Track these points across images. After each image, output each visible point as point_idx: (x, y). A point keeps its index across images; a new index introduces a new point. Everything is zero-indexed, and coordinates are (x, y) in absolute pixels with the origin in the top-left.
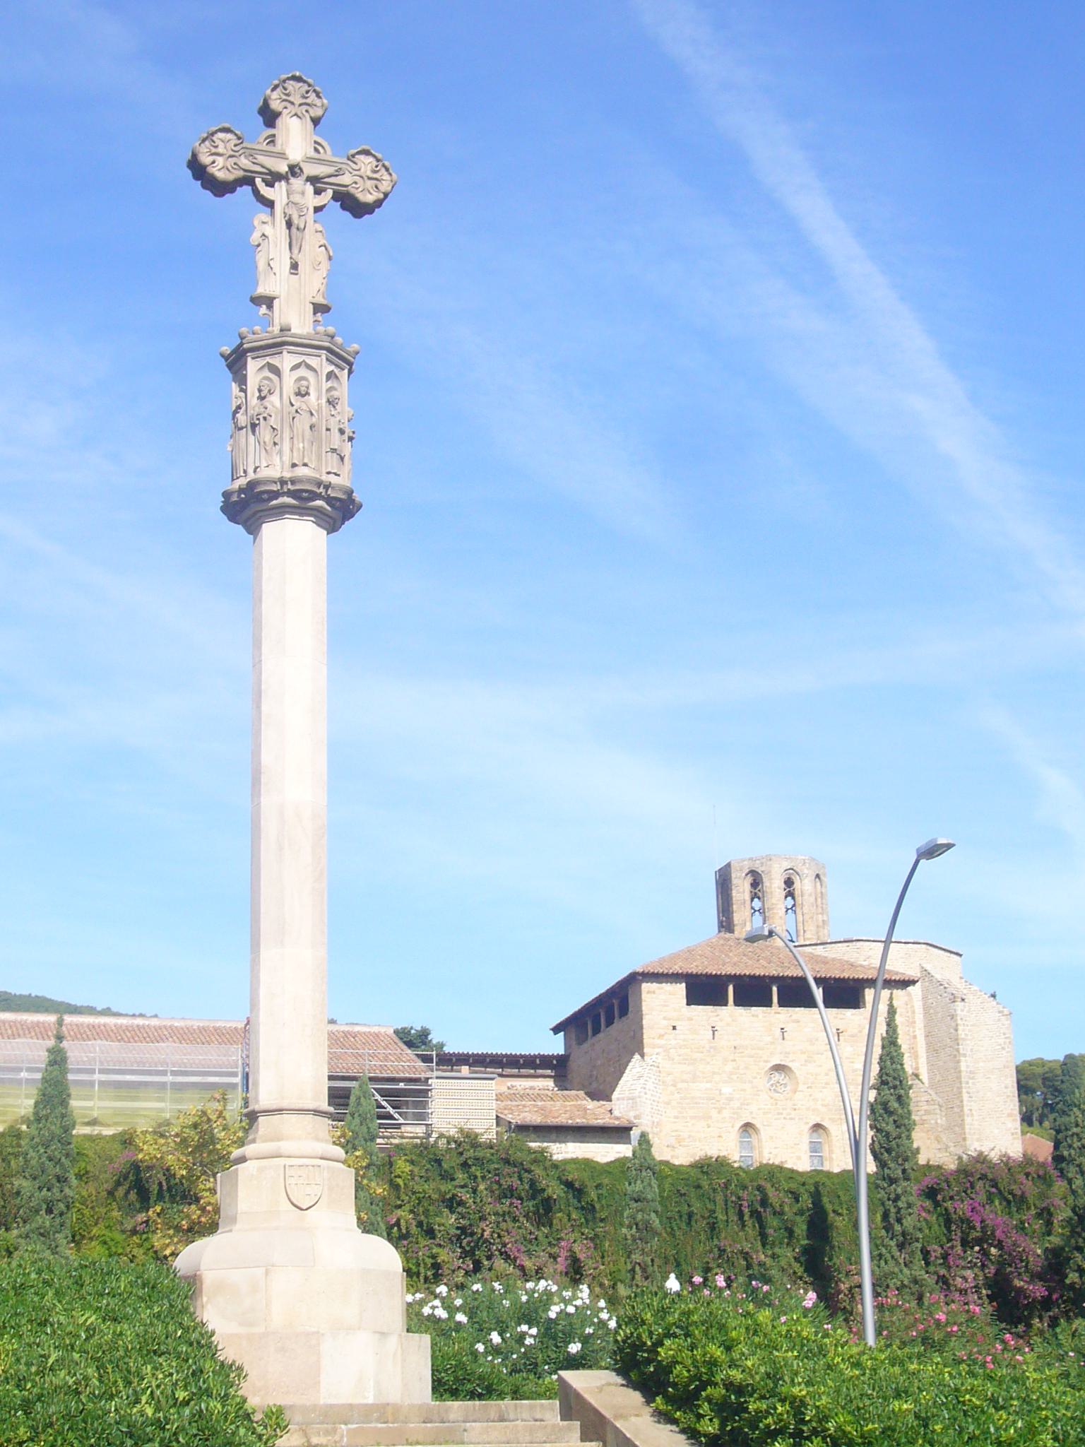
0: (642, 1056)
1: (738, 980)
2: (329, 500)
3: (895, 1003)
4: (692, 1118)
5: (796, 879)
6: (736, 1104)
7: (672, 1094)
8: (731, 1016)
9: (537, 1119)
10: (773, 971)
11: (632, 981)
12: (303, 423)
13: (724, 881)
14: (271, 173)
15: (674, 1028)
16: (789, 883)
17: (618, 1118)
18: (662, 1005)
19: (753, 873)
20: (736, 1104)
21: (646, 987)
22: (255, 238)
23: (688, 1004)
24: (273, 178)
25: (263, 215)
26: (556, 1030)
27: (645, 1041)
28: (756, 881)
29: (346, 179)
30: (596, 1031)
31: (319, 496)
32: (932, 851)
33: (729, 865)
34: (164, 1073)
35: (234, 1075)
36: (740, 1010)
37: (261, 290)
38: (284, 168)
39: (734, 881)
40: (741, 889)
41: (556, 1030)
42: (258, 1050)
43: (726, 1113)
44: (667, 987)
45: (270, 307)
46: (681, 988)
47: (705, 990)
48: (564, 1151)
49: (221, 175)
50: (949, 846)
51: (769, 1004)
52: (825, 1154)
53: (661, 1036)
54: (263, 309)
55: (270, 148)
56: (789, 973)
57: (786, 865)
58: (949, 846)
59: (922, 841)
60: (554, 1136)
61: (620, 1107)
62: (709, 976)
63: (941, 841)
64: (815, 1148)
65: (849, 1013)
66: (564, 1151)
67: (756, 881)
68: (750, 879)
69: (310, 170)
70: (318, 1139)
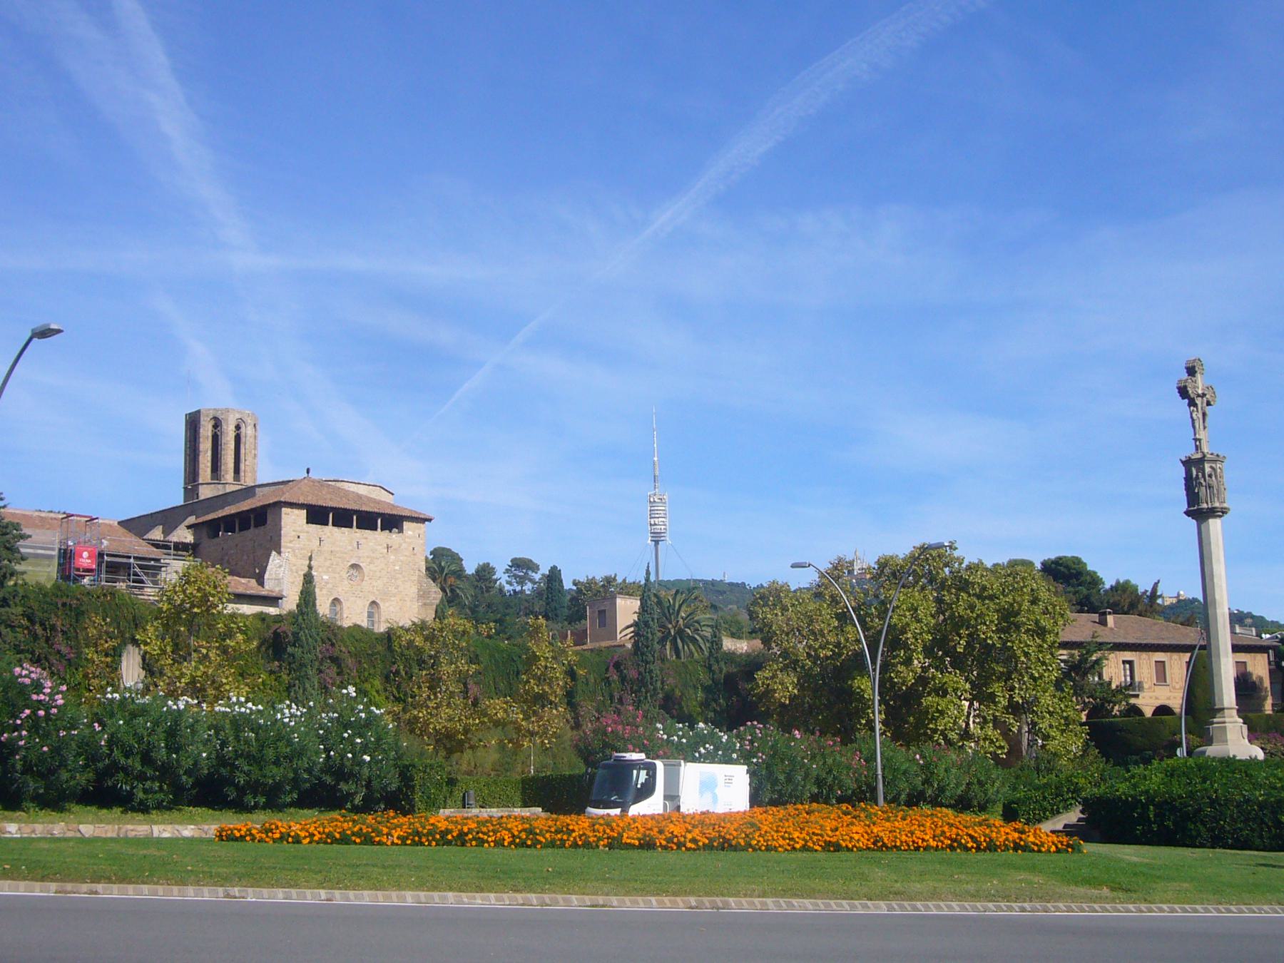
0: (279, 553)
1: (382, 515)
5: (243, 426)
6: (330, 586)
8: (330, 532)
10: (330, 504)
13: (193, 423)
16: (238, 427)
18: (293, 521)
19: (215, 418)
20: (330, 586)
21: (284, 510)
27: (283, 544)
28: (217, 423)
32: (45, 333)
33: (199, 412)
35: (53, 549)
36: (336, 529)
39: (202, 423)
40: (206, 431)
42: (1210, 544)
44: (296, 511)
47: (317, 515)
50: (59, 331)
51: (351, 527)
52: (376, 619)
57: (238, 416)
58: (59, 331)
59: (39, 323)
61: (270, 587)
62: (345, 510)
63: (53, 326)
64: (370, 615)
67: (217, 423)
68: (213, 422)
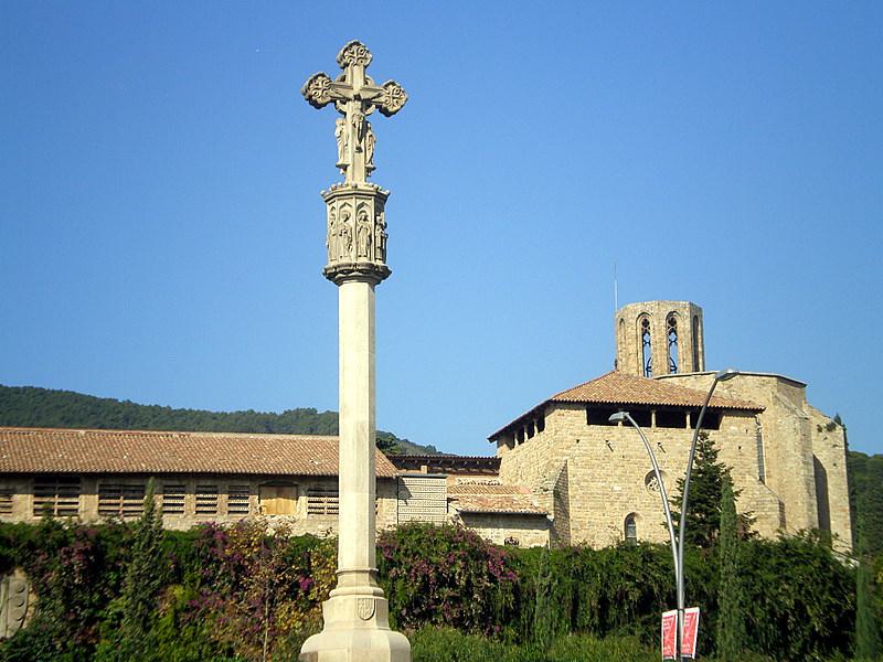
2: (359, 271)
3: (550, 420)
4: (591, 508)
7: (577, 490)
9: (474, 507)
11: (550, 405)
12: (363, 237)
14: (344, 98)
15: (578, 441)
17: (536, 508)
20: (624, 499)
22: (337, 133)
23: (589, 424)
24: (345, 100)
25: (340, 121)
26: (491, 439)
29: (382, 99)
30: (521, 441)
31: (353, 271)
34: (703, 346)
37: (340, 163)
38: (351, 96)
41: (491, 439)
43: (617, 505)
45: (345, 170)
46: (583, 414)
47: (599, 414)
48: (496, 536)
49: (320, 101)
53: (568, 447)
54: (342, 171)
55: (342, 83)
56: (664, 402)
60: (489, 521)
65: (672, 431)
66: (496, 536)
69: (364, 96)
70: (371, 585)
